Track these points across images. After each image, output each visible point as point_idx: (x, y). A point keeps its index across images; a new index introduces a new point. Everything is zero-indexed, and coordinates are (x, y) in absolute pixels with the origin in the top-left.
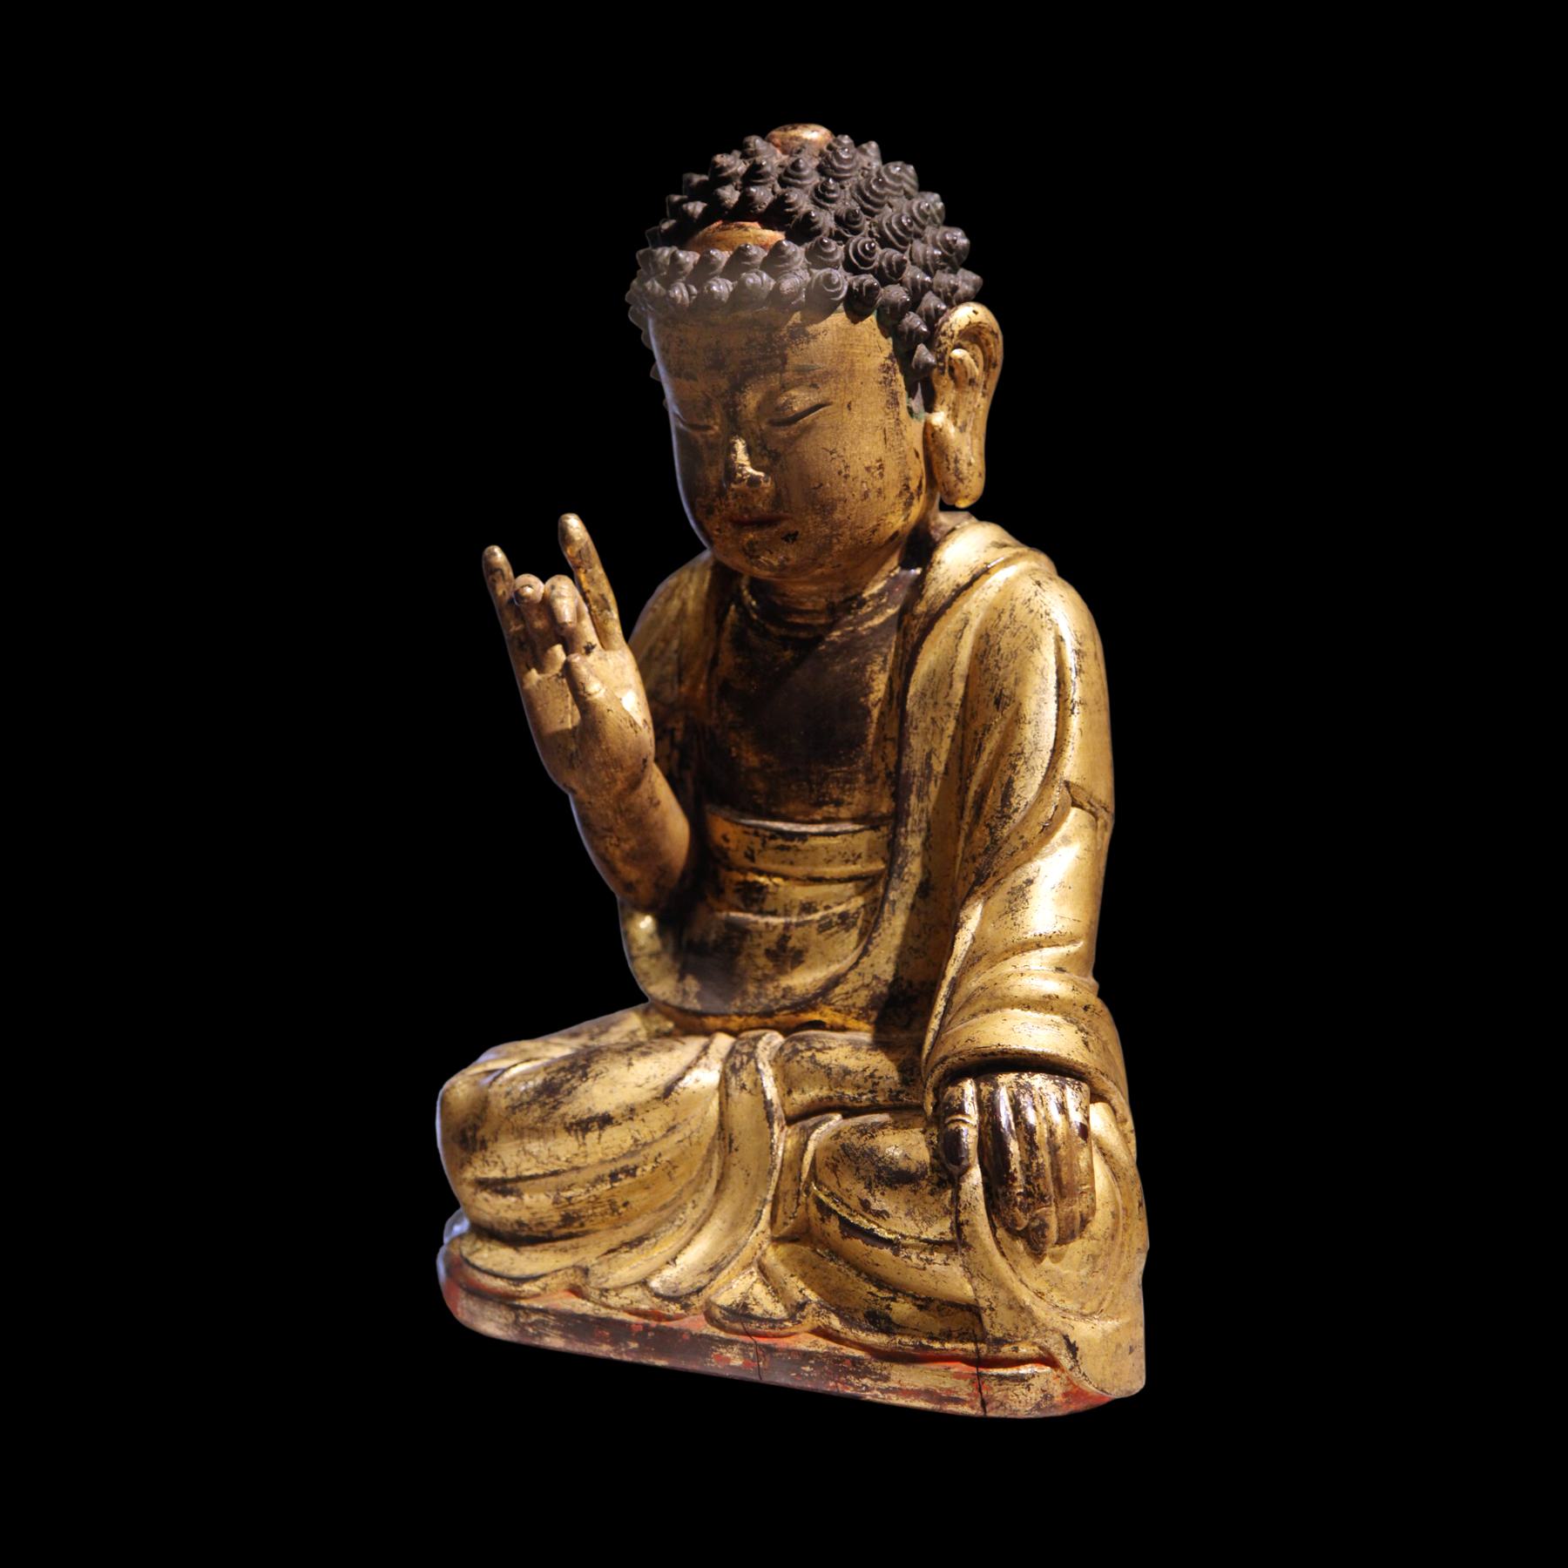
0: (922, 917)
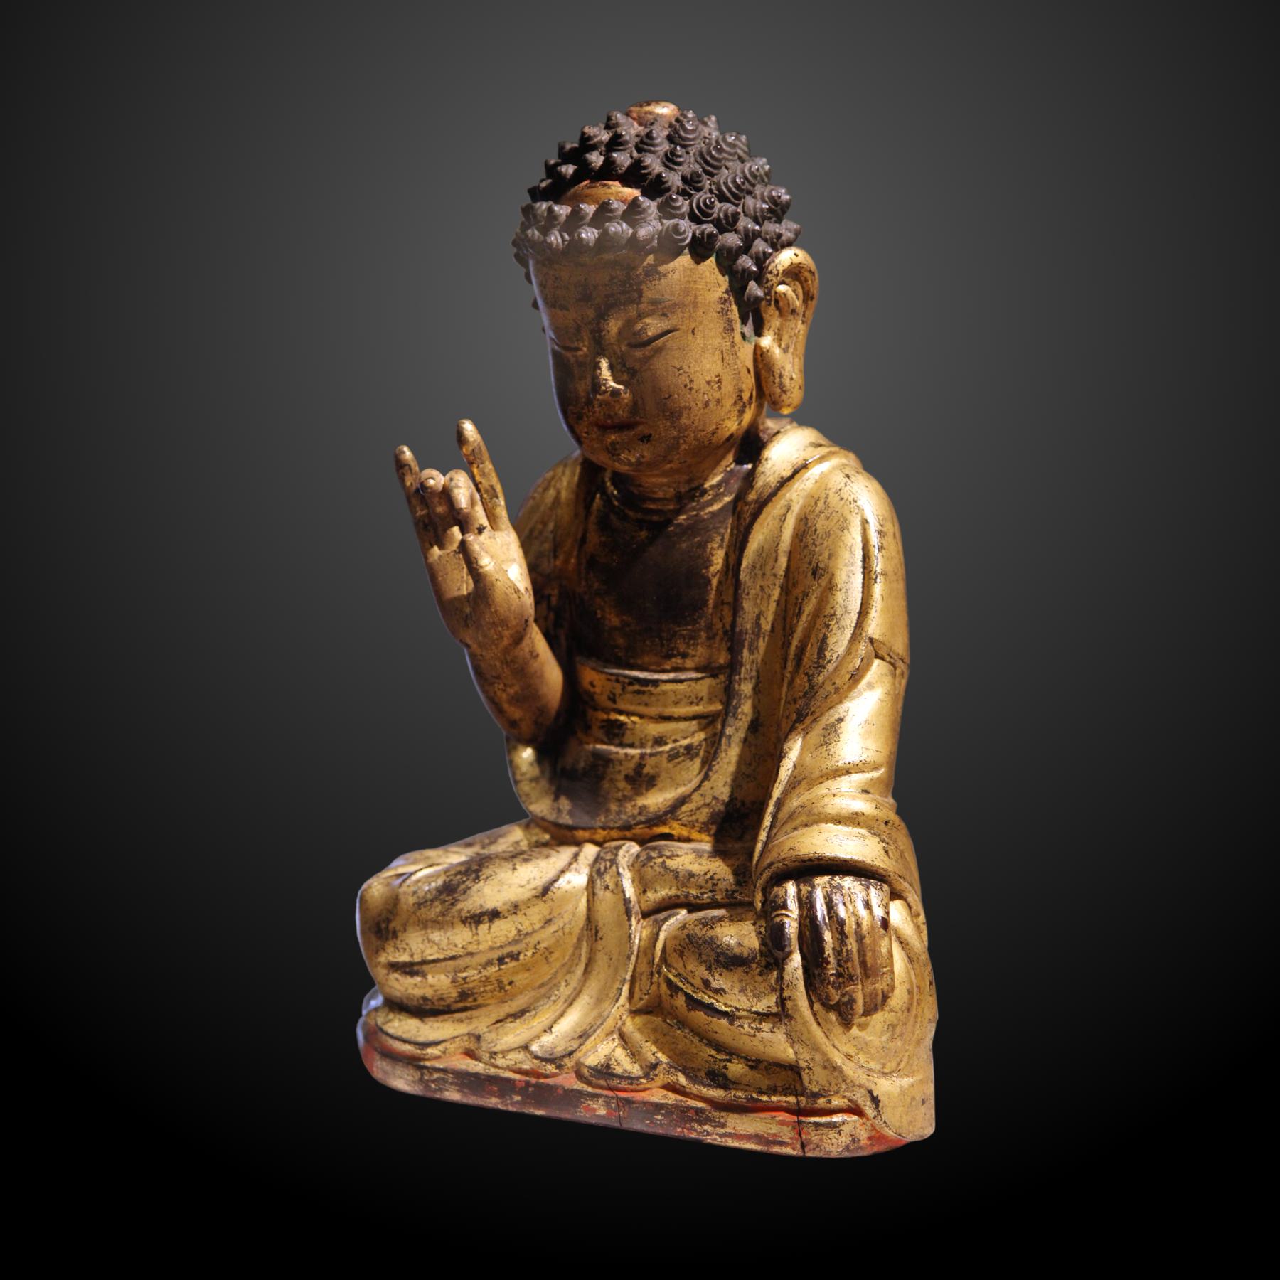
0: (753, 749)
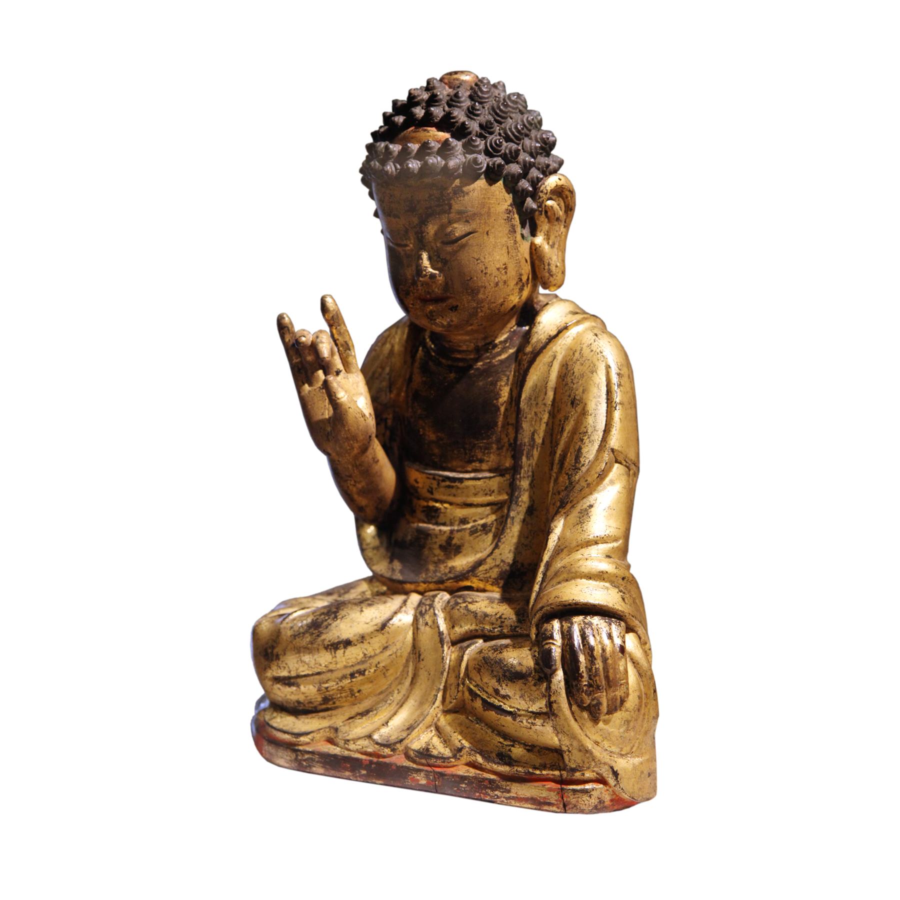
0: (529, 526)
